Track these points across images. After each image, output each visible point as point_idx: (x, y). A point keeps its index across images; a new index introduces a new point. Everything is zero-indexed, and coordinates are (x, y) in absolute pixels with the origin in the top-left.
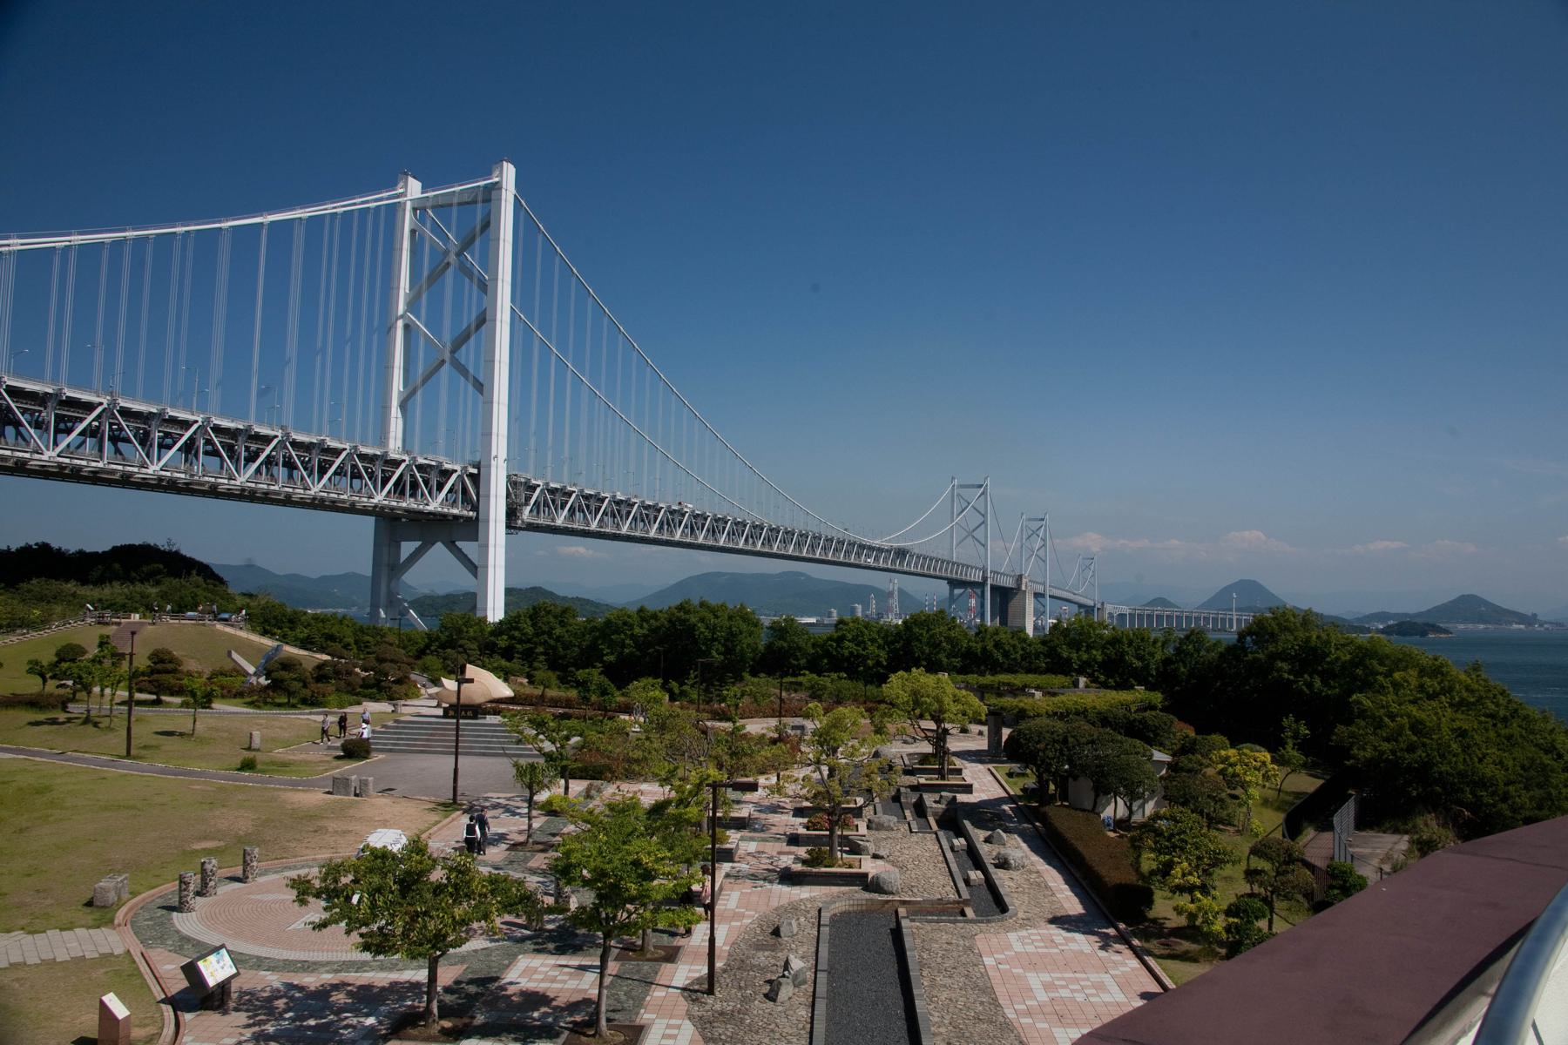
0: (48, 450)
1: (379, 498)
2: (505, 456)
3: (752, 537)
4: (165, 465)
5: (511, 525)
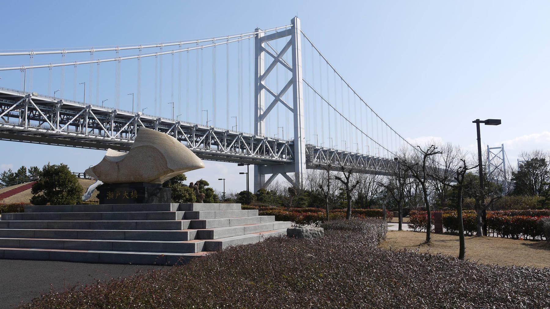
5: (308, 167)
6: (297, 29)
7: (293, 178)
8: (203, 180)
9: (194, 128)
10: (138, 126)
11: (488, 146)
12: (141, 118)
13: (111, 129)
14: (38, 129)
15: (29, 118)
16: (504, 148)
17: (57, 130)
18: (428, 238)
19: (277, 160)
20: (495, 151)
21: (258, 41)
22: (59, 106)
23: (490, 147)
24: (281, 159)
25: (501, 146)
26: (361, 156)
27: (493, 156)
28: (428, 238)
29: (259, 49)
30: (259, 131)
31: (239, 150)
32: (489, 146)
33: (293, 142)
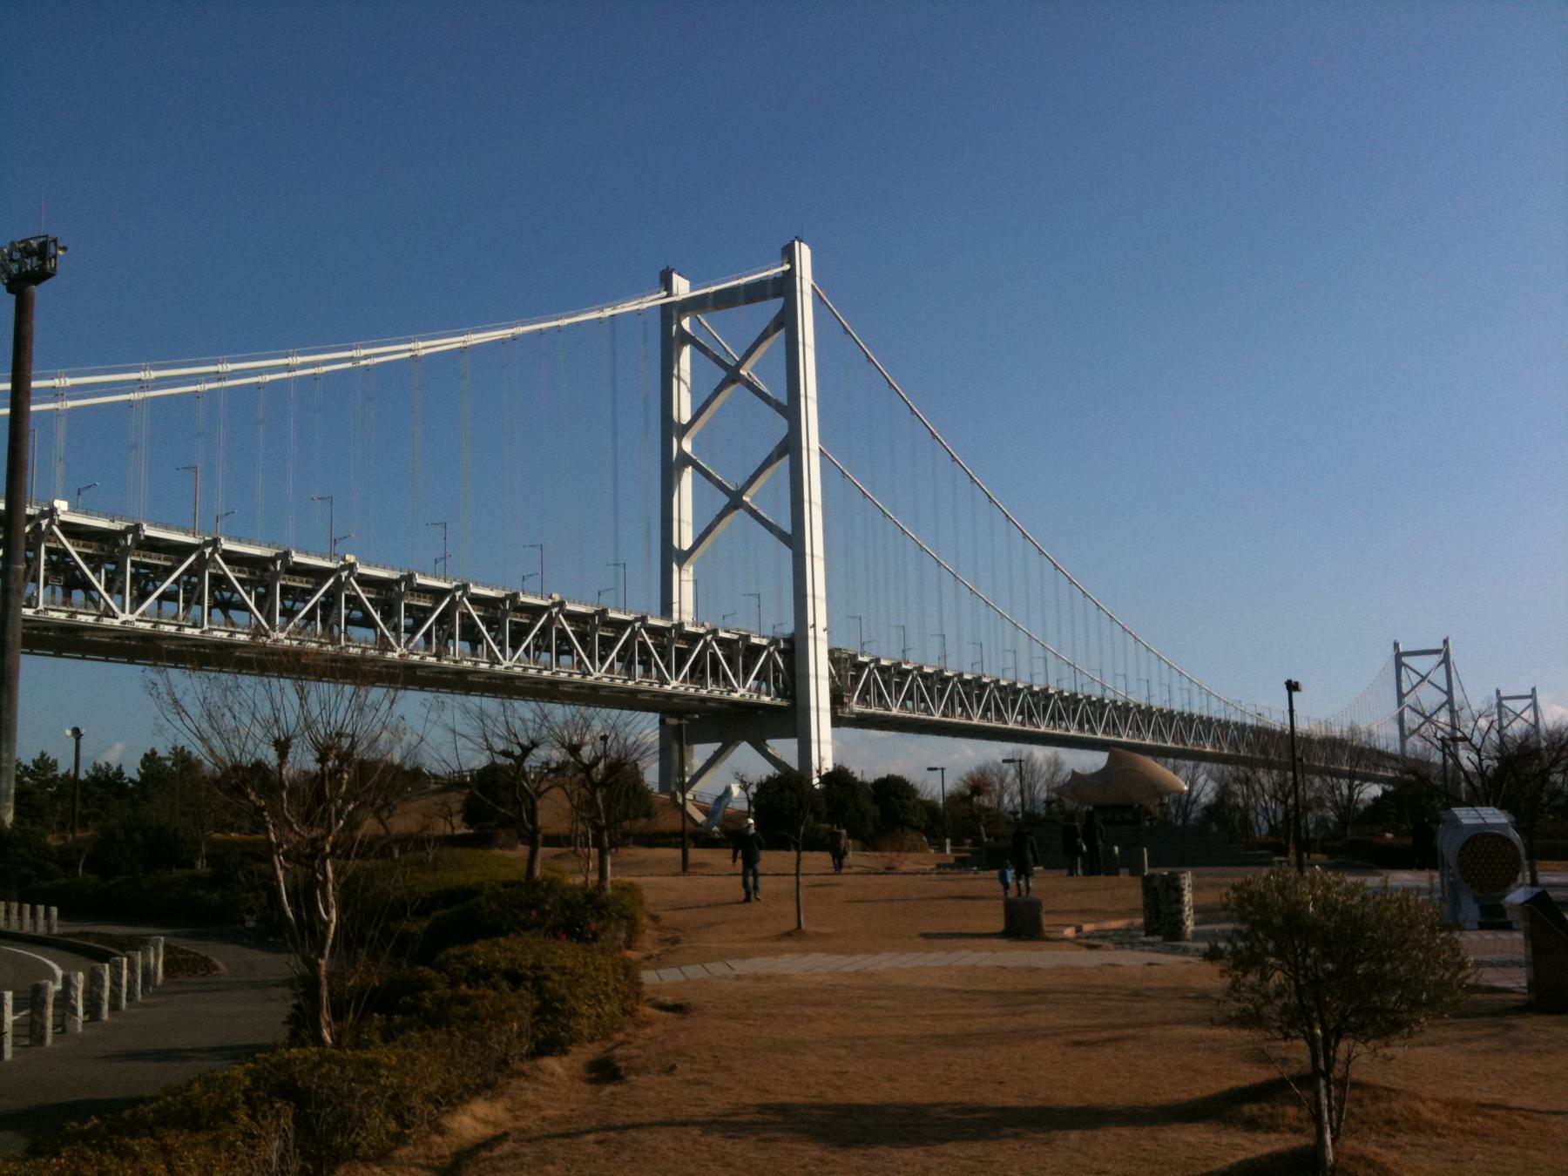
0: (123, 611)
1: (674, 685)
2: (824, 625)
3: (1089, 722)
4: (143, 614)
5: (837, 721)
9: (508, 602)
10: (49, 551)
11: (1396, 645)
12: (225, 551)
13: (34, 576)
14: (156, 624)
16: (1452, 652)
17: (124, 617)
20: (1424, 664)
21: (1398, 656)
23: (1503, 694)
25: (1440, 646)
27: (1415, 679)
29: (1399, 665)
30: (675, 607)
31: (458, 647)
32: (1400, 646)
33: (790, 640)
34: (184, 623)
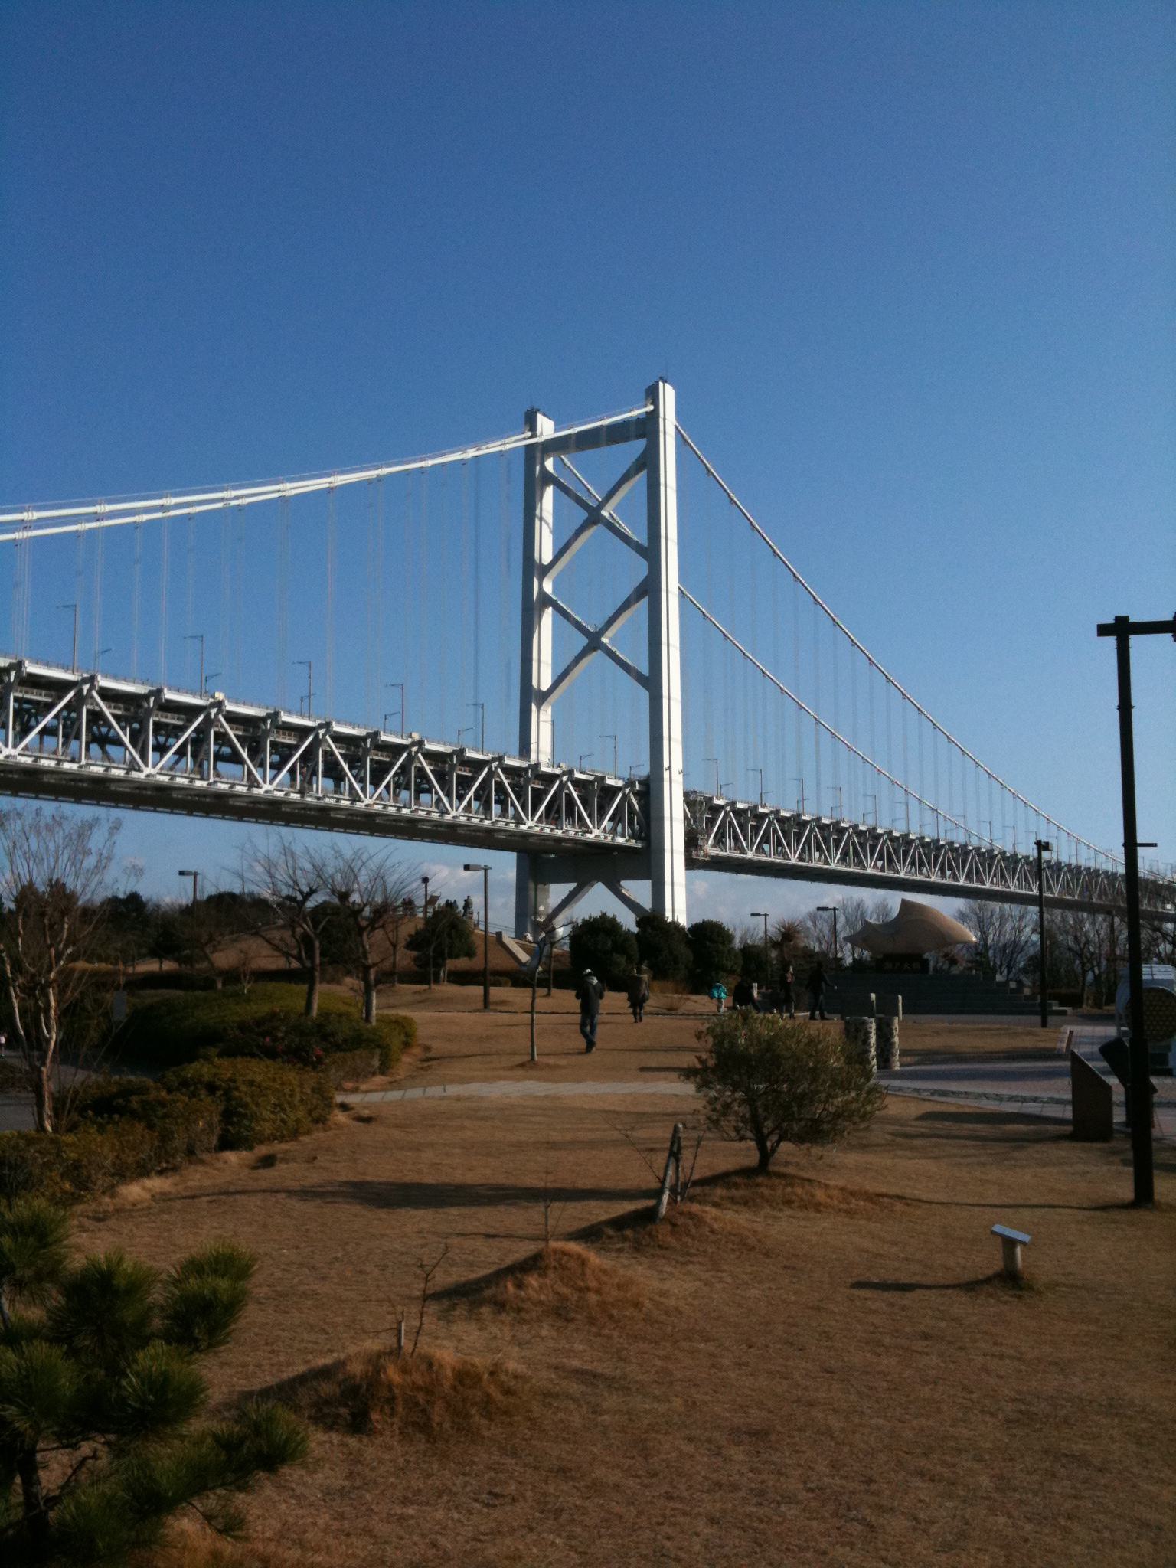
5: (691, 864)
6: (664, 419)
7: (647, 903)
8: (619, 920)
15: (218, 757)
17: (148, 770)
18: (765, 1156)
19: (596, 840)
22: (12, 679)
24: (512, 826)
26: (772, 816)
28: (765, 1156)
30: (533, 747)
31: (322, 784)
33: (646, 783)
34: (63, 758)
